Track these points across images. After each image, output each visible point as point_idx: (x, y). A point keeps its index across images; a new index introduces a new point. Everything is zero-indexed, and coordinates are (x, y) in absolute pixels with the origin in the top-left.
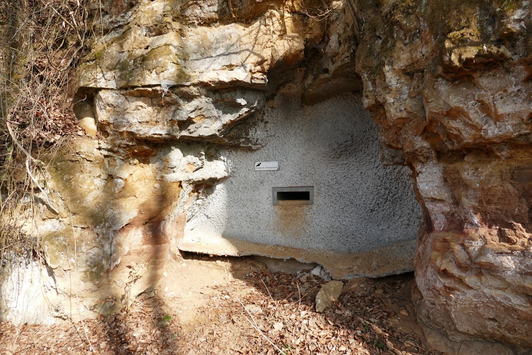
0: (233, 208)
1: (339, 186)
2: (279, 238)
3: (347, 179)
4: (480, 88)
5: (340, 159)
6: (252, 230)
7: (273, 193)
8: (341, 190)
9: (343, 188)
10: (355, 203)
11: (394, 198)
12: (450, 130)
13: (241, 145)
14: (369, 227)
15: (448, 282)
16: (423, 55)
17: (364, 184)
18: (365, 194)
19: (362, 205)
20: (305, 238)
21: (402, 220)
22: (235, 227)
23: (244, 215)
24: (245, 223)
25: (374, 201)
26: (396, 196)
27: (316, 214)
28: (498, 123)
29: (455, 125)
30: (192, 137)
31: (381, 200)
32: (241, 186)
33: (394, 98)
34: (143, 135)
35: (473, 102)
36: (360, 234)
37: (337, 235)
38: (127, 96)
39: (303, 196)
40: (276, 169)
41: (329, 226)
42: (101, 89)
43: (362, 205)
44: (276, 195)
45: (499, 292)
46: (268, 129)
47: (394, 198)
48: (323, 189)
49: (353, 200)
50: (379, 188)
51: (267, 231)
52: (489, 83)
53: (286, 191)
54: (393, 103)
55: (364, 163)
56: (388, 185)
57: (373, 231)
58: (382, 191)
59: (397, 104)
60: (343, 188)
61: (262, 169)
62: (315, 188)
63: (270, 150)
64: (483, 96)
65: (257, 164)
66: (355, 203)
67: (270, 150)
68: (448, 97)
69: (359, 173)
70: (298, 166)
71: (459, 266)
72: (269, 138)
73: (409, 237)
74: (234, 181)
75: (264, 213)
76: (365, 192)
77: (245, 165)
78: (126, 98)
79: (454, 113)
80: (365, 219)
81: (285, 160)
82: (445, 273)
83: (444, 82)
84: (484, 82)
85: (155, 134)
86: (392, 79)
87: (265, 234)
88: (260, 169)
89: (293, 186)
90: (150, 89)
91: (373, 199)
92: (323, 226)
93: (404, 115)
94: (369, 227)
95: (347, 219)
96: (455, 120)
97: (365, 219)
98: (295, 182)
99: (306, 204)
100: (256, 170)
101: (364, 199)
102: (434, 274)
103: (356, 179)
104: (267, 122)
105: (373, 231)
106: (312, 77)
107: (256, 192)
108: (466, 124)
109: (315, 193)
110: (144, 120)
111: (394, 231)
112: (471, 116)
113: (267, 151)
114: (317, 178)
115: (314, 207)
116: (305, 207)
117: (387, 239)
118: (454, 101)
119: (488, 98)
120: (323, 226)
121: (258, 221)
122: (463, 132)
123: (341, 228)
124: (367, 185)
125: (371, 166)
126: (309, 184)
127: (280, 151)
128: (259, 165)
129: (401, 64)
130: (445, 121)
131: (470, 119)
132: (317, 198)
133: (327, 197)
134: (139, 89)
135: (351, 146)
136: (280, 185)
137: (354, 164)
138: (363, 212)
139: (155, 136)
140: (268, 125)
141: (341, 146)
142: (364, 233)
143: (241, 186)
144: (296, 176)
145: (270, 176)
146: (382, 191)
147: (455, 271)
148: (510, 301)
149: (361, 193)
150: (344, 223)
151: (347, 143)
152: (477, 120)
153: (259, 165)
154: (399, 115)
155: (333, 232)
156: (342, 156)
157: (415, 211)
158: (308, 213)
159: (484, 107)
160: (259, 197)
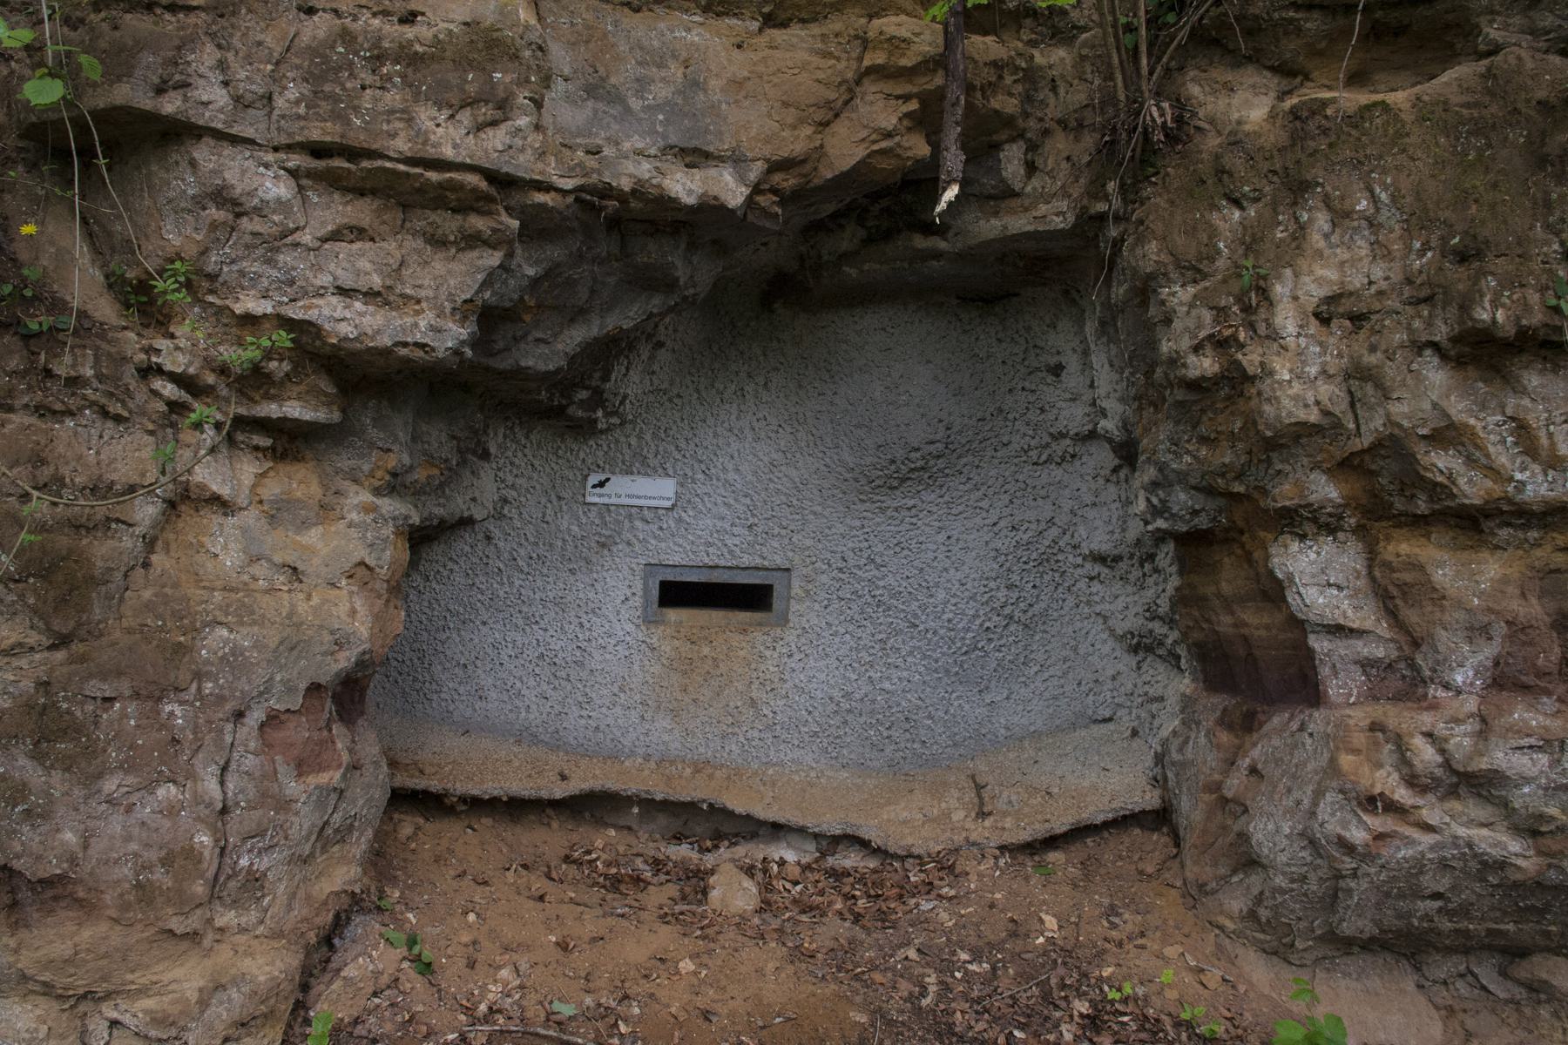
0: (484, 630)
1: (876, 572)
2: (663, 733)
3: (906, 552)
4: (1524, 392)
5: (898, 493)
6: (558, 708)
7: (645, 585)
8: (881, 583)
9: (890, 580)
10: (921, 627)
11: (1030, 614)
12: (1426, 469)
13: (571, 410)
14: (959, 697)
15: (1378, 823)
16: (1370, 283)
17: (952, 571)
18: (953, 601)
19: (942, 632)
20: (756, 734)
21: (1046, 675)
22: (493, 695)
23: (532, 653)
24: (532, 683)
25: (978, 622)
26: (1036, 609)
27: (797, 657)
28: (1551, 473)
29: (1441, 462)
30: (487, 369)
31: (995, 618)
32: (522, 552)
33: (1291, 371)
34: (356, 339)
35: (1499, 418)
36: (930, 717)
37: (862, 720)
38: (304, 182)
39: (750, 597)
40: (668, 504)
41: (837, 694)
42: (197, 132)
43: (942, 632)
44: (655, 593)
45: (1485, 832)
46: (656, 367)
47: (1030, 614)
48: (824, 578)
49: (916, 616)
50: (992, 584)
51: (618, 710)
52: (1543, 386)
53: (703, 579)
54: (1290, 382)
55: (961, 508)
56: (1015, 578)
57: (967, 707)
58: (1000, 595)
59: (1297, 388)
60: (890, 580)
61: (614, 500)
62: (794, 574)
63: (648, 437)
64: (1526, 409)
65: (594, 479)
66: (921, 627)
67: (648, 437)
68: (1448, 397)
69: (941, 537)
70: (748, 501)
71: (1412, 781)
72: (651, 398)
73: (1058, 722)
74: (496, 533)
75: (610, 648)
76: (954, 596)
77: (545, 480)
78: (301, 188)
79: (1447, 435)
80: (947, 671)
81: (700, 476)
82: (1371, 802)
83: (1436, 360)
84: (1533, 380)
85: (405, 344)
86: (1287, 320)
87: (610, 721)
88: (606, 500)
89: (722, 563)
90: (433, 176)
91: (976, 616)
92: (819, 694)
93: (1313, 416)
94: (959, 697)
95: (895, 674)
96: (1446, 450)
97: (947, 671)
98: (731, 552)
99: (760, 624)
100: (589, 499)
101: (951, 616)
102: (1342, 808)
103: (931, 555)
104: (660, 345)
105: (967, 707)
106: (862, 233)
107: (579, 576)
108: (1470, 461)
109: (796, 590)
110: (362, 284)
111: (1020, 708)
112: (1491, 449)
113: (633, 441)
114: (809, 542)
115: (791, 636)
116: (759, 637)
117: (1003, 731)
118: (1458, 408)
119: (1536, 415)
120: (819, 694)
121: (584, 675)
122: (1462, 481)
123: (873, 701)
124: (959, 575)
125: (978, 520)
126: (779, 561)
127: (683, 445)
128: (601, 484)
129: (1313, 292)
130: (1420, 449)
131: (1488, 456)
132: (803, 609)
133: (836, 605)
134: (388, 165)
135: (939, 457)
136: (676, 559)
137: (935, 509)
138: (943, 654)
139: (403, 352)
140: (663, 355)
141: (914, 455)
142: (941, 714)
143: (522, 552)
144: (736, 530)
145: (638, 524)
146: (1000, 595)
147: (1402, 795)
148: (1505, 848)
149: (941, 595)
150: (887, 685)
151: (932, 448)
152: (1503, 460)
153: (601, 484)
154: (1302, 415)
155: (849, 711)
156: (909, 483)
157: (1081, 652)
158: (768, 653)
159: (1522, 429)
160: (591, 595)
